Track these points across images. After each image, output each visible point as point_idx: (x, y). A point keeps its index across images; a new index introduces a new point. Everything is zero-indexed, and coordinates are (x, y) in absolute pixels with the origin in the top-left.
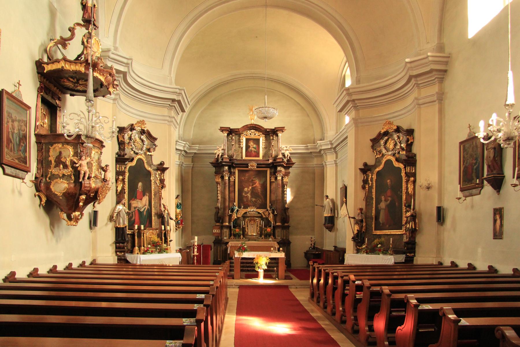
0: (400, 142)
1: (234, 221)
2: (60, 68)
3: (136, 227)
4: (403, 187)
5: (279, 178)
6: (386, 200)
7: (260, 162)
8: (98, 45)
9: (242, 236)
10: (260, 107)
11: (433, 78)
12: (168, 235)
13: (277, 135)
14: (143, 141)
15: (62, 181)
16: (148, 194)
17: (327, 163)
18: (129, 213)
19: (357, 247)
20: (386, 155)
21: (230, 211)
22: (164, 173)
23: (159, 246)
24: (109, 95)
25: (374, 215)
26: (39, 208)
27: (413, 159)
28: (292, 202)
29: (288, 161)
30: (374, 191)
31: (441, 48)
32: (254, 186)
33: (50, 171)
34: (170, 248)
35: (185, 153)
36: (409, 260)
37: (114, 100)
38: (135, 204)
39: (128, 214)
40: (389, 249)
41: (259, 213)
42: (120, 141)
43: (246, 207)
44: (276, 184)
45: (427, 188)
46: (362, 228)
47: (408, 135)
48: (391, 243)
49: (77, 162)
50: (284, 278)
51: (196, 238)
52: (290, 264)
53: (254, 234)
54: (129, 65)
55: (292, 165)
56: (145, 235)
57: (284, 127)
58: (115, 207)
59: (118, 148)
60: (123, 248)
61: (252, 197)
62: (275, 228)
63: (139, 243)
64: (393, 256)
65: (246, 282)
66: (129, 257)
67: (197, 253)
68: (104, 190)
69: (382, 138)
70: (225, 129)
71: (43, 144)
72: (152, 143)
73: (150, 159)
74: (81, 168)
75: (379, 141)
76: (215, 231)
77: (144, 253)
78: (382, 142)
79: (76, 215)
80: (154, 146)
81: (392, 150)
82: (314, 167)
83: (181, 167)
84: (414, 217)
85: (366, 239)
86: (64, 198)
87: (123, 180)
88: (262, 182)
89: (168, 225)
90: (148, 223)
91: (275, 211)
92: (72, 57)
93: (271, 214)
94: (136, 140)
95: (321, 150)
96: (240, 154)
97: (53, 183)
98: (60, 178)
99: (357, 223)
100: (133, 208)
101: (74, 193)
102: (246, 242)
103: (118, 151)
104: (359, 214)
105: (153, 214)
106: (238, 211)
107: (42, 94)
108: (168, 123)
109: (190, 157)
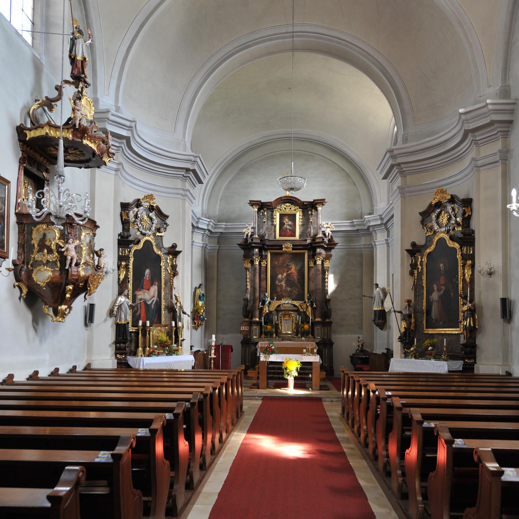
0: (456, 214)
1: (266, 315)
2: (44, 134)
3: (140, 323)
4: (459, 272)
5: (319, 262)
6: (439, 290)
7: (296, 243)
8: (91, 107)
9: (274, 335)
10: (284, 176)
11: (496, 132)
12: (179, 333)
13: (316, 210)
14: (151, 219)
15: (46, 269)
16: (157, 283)
17: (377, 243)
18: (133, 306)
19: (404, 350)
20: (438, 231)
21: (260, 303)
22: (176, 258)
23: (167, 346)
24: (104, 166)
25: (425, 308)
26: (19, 301)
27: (471, 237)
28: (335, 292)
29: (329, 240)
30: (424, 277)
31: (505, 92)
32: (289, 272)
33: (33, 256)
34: (182, 349)
35: (210, 233)
36: (469, 368)
37: (117, 170)
38: (140, 295)
39: (131, 307)
40: (443, 353)
41: (295, 306)
42: (123, 220)
43: (279, 299)
44: (315, 270)
45: (489, 274)
46: (411, 326)
47: (464, 207)
48: (445, 345)
49: (63, 246)
50: (319, 389)
51: (214, 336)
52: (333, 370)
53: (289, 332)
54: (132, 129)
55: (334, 246)
56: (151, 332)
57: (324, 200)
58: (117, 299)
59: (122, 229)
60: (125, 349)
61: (287, 286)
62: (314, 324)
63: (144, 343)
64: (446, 362)
65: (272, 392)
66: (131, 360)
67: (215, 355)
68: (95, 279)
69: (433, 211)
70: (255, 203)
71: (25, 225)
72: (162, 222)
73: (160, 240)
74: (68, 253)
75: (430, 215)
76: (242, 328)
77: (149, 356)
78: (434, 216)
79: (62, 309)
80: (165, 226)
81: (446, 226)
82: (361, 248)
83: (205, 250)
84: (472, 312)
85: (415, 339)
86: (48, 289)
87: (127, 267)
88: (298, 268)
89: (180, 321)
90: (156, 318)
91: (314, 304)
92: (60, 121)
93: (309, 307)
94: (143, 219)
95: (369, 227)
96: (273, 234)
97: (35, 271)
98: (44, 265)
99: (403, 319)
100: (139, 300)
101: (59, 282)
102: (274, 342)
103: (122, 231)
104: (406, 308)
105: (162, 308)
106: (270, 303)
107: (25, 165)
108: (182, 197)
109: (215, 237)
